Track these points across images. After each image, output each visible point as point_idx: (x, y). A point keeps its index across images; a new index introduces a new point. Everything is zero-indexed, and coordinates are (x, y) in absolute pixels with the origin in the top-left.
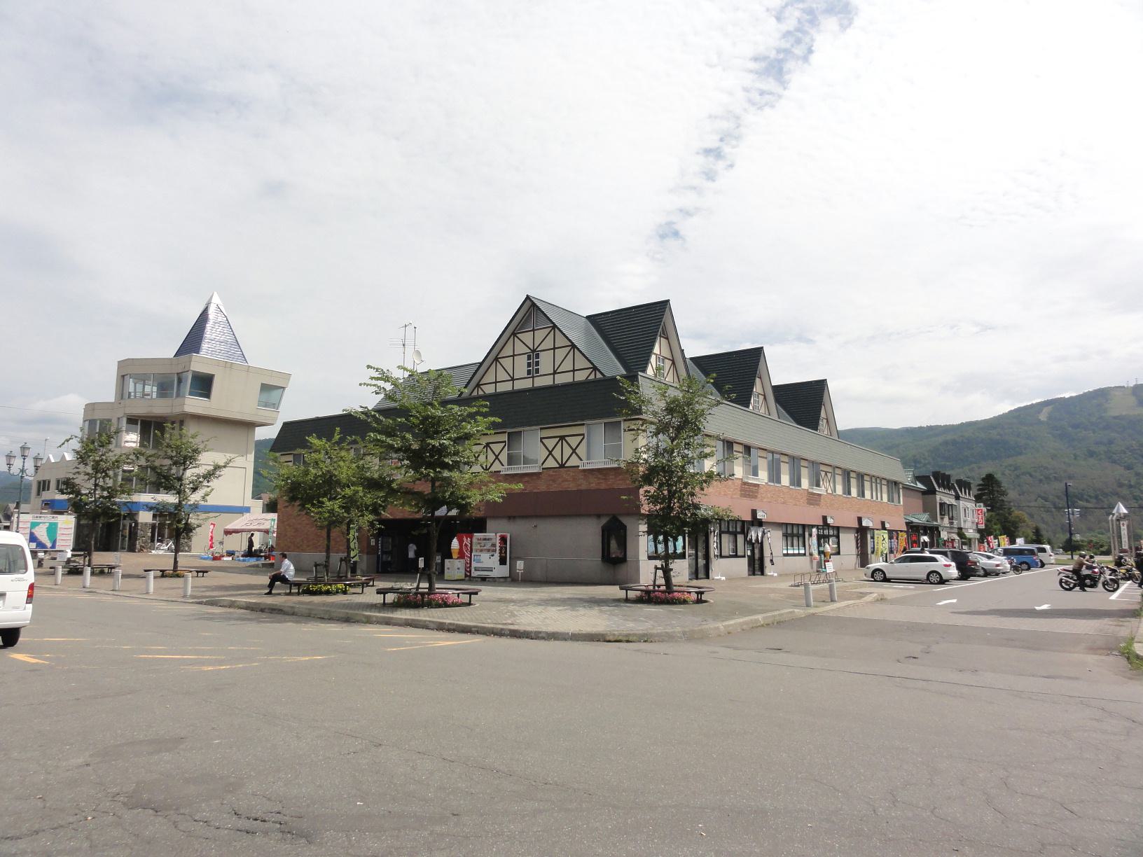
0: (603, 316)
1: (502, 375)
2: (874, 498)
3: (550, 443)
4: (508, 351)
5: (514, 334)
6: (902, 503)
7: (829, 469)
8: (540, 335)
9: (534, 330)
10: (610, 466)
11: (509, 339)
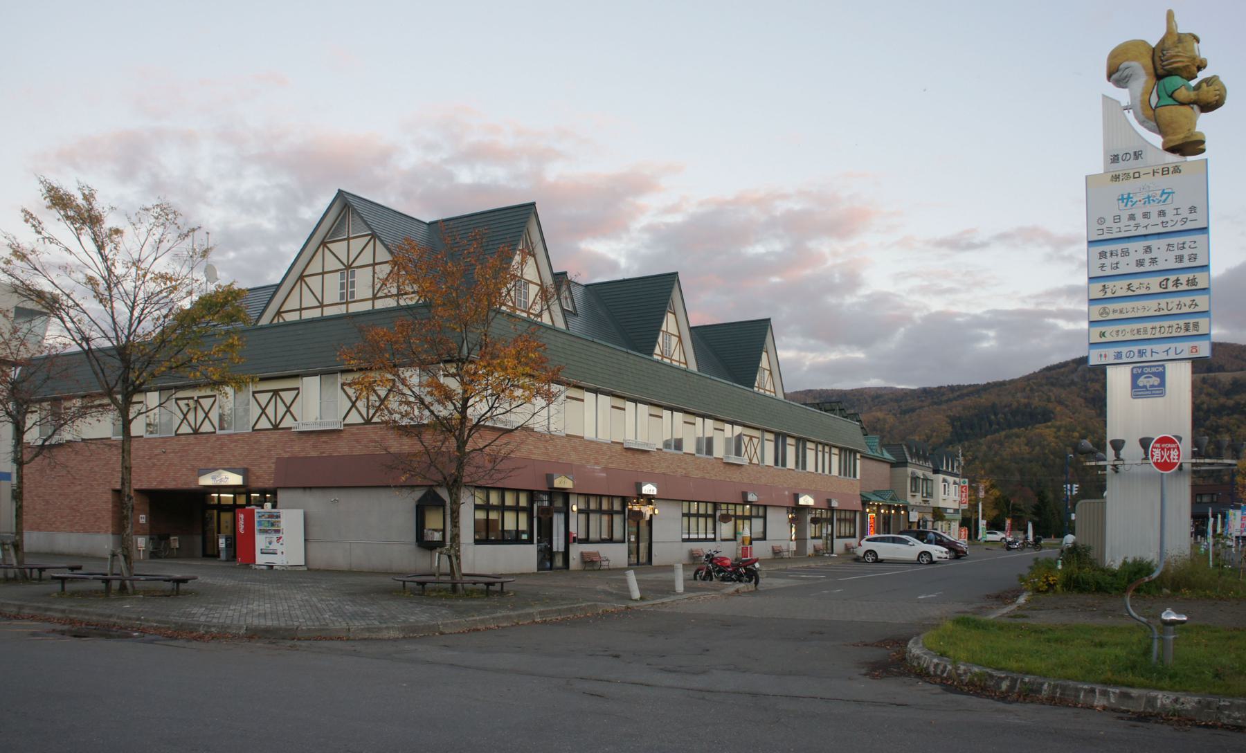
0: (497, 213)
1: (309, 301)
2: (820, 471)
3: (263, 398)
4: (315, 267)
5: (324, 244)
6: (858, 476)
7: (757, 433)
8: (357, 245)
9: (348, 239)
10: (323, 429)
11: (317, 251)
